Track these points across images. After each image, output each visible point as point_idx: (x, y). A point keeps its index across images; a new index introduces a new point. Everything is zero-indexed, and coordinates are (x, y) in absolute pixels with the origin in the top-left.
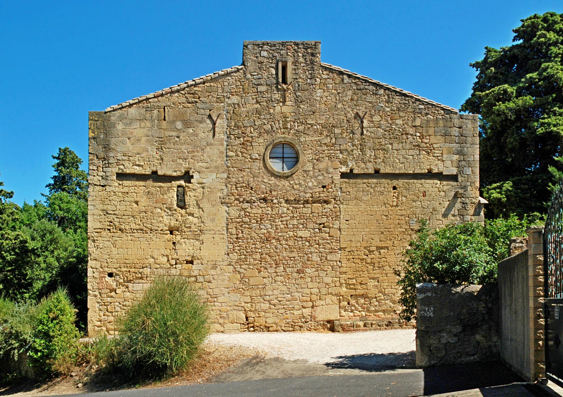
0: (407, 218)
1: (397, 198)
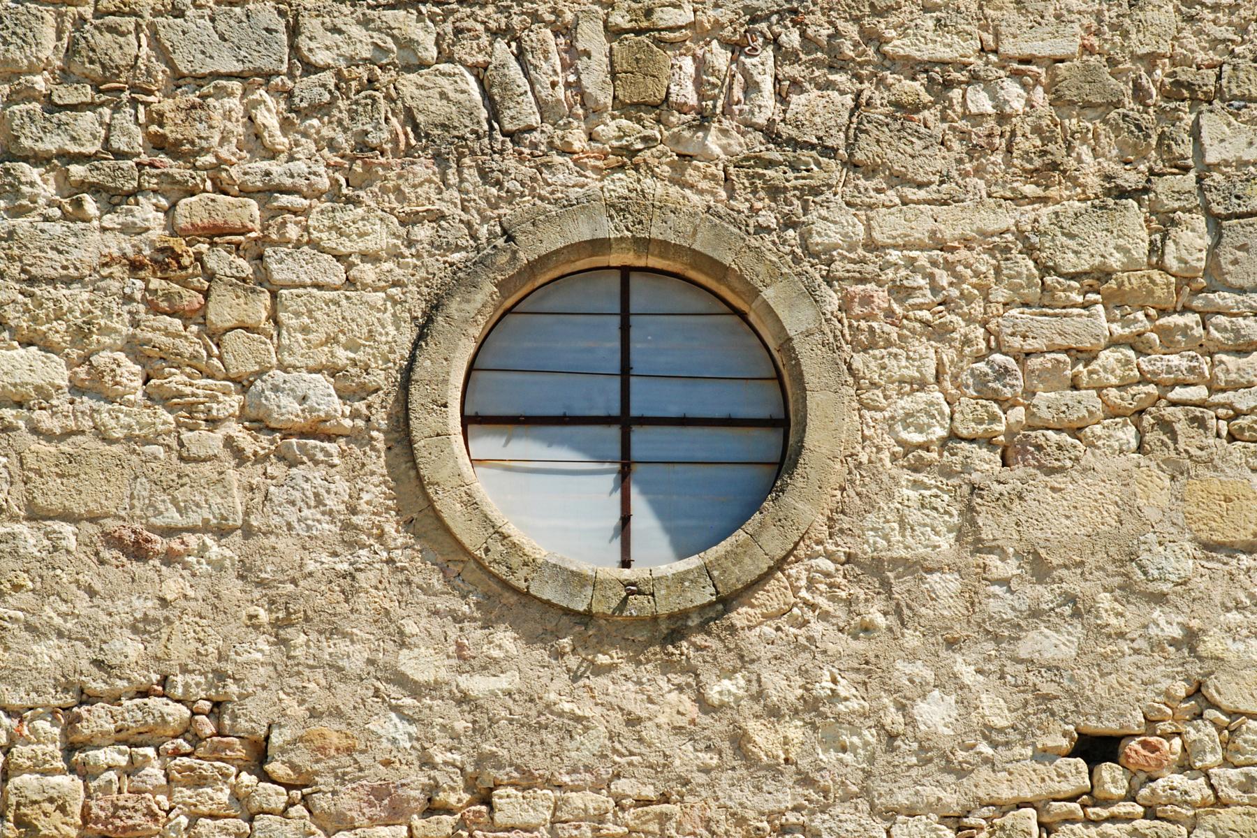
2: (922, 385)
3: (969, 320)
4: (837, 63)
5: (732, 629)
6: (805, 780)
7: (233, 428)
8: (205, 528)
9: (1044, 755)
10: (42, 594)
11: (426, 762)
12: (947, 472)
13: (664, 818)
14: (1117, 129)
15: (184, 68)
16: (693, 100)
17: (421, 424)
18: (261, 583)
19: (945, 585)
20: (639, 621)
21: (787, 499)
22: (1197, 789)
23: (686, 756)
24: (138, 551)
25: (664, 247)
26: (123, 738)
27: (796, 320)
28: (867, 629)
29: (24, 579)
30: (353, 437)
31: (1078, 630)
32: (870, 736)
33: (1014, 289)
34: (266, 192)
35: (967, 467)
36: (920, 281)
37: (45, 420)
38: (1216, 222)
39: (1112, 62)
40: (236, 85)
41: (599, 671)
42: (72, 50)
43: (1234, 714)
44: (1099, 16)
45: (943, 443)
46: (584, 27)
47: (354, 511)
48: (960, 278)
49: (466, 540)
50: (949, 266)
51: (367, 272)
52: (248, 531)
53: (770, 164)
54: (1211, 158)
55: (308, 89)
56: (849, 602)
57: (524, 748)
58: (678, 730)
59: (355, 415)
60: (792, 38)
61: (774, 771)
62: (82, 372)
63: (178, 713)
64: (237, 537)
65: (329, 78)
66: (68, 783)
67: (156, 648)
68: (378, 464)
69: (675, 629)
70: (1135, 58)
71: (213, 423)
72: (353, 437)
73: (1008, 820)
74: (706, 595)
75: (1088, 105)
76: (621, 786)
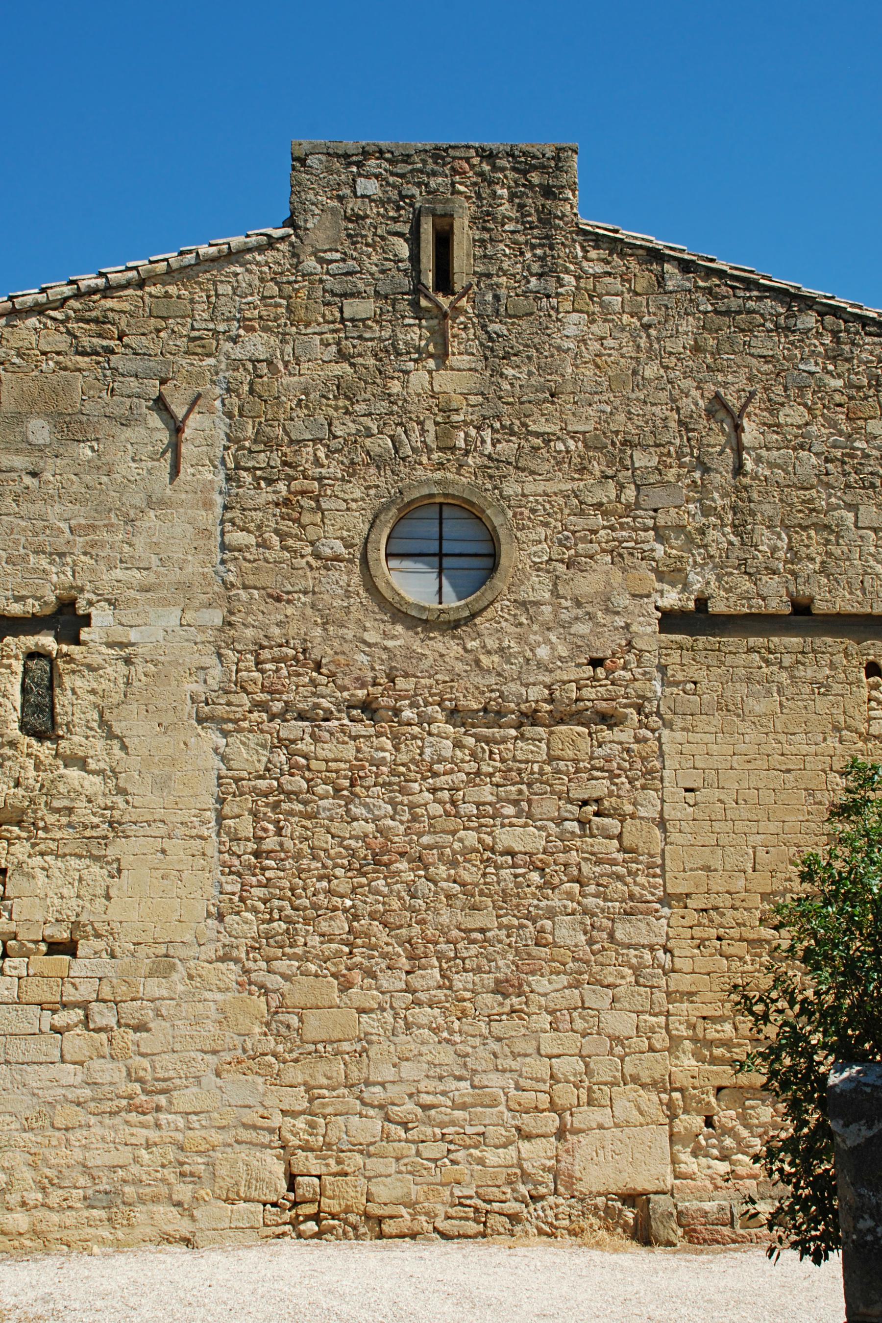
2: (540, 542)
3: (556, 520)
4: (512, 433)
5: (475, 625)
6: (499, 675)
7: (310, 559)
8: (300, 592)
9: (578, 665)
10: (247, 613)
11: (373, 669)
12: (548, 572)
13: (452, 687)
14: (605, 456)
15: (293, 438)
16: (463, 446)
17: (371, 556)
18: (318, 610)
19: (547, 609)
20: (444, 623)
21: (494, 581)
22: (628, 675)
23: (459, 667)
24: (278, 599)
25: (453, 496)
26: (274, 660)
27: (497, 521)
28: (521, 624)
29: (242, 608)
30: (350, 561)
31: (591, 624)
32: (521, 660)
33: (571, 509)
34: (320, 479)
35: (555, 570)
36: (540, 507)
37: (247, 555)
38: (638, 487)
39: (604, 433)
40: (311, 443)
41: (431, 639)
42: (257, 433)
43: (641, 651)
44: (600, 417)
45: (547, 562)
46: (427, 422)
47: (349, 586)
48: (553, 506)
49: (386, 595)
50: (549, 502)
51: (354, 505)
52: (314, 593)
53: (490, 468)
54: (636, 466)
55: (334, 444)
56: (515, 615)
57: (405, 664)
58: (457, 658)
59: (349, 553)
60: (497, 425)
61: (489, 671)
62: (260, 539)
63: (292, 652)
64: (310, 595)
65: (341, 440)
66: (256, 675)
67: (284, 631)
68: (357, 570)
69: (456, 624)
70: (612, 432)
71: (302, 556)
72: (350, 561)
73: (566, 687)
74: (467, 613)
75: (596, 448)
76: (438, 677)
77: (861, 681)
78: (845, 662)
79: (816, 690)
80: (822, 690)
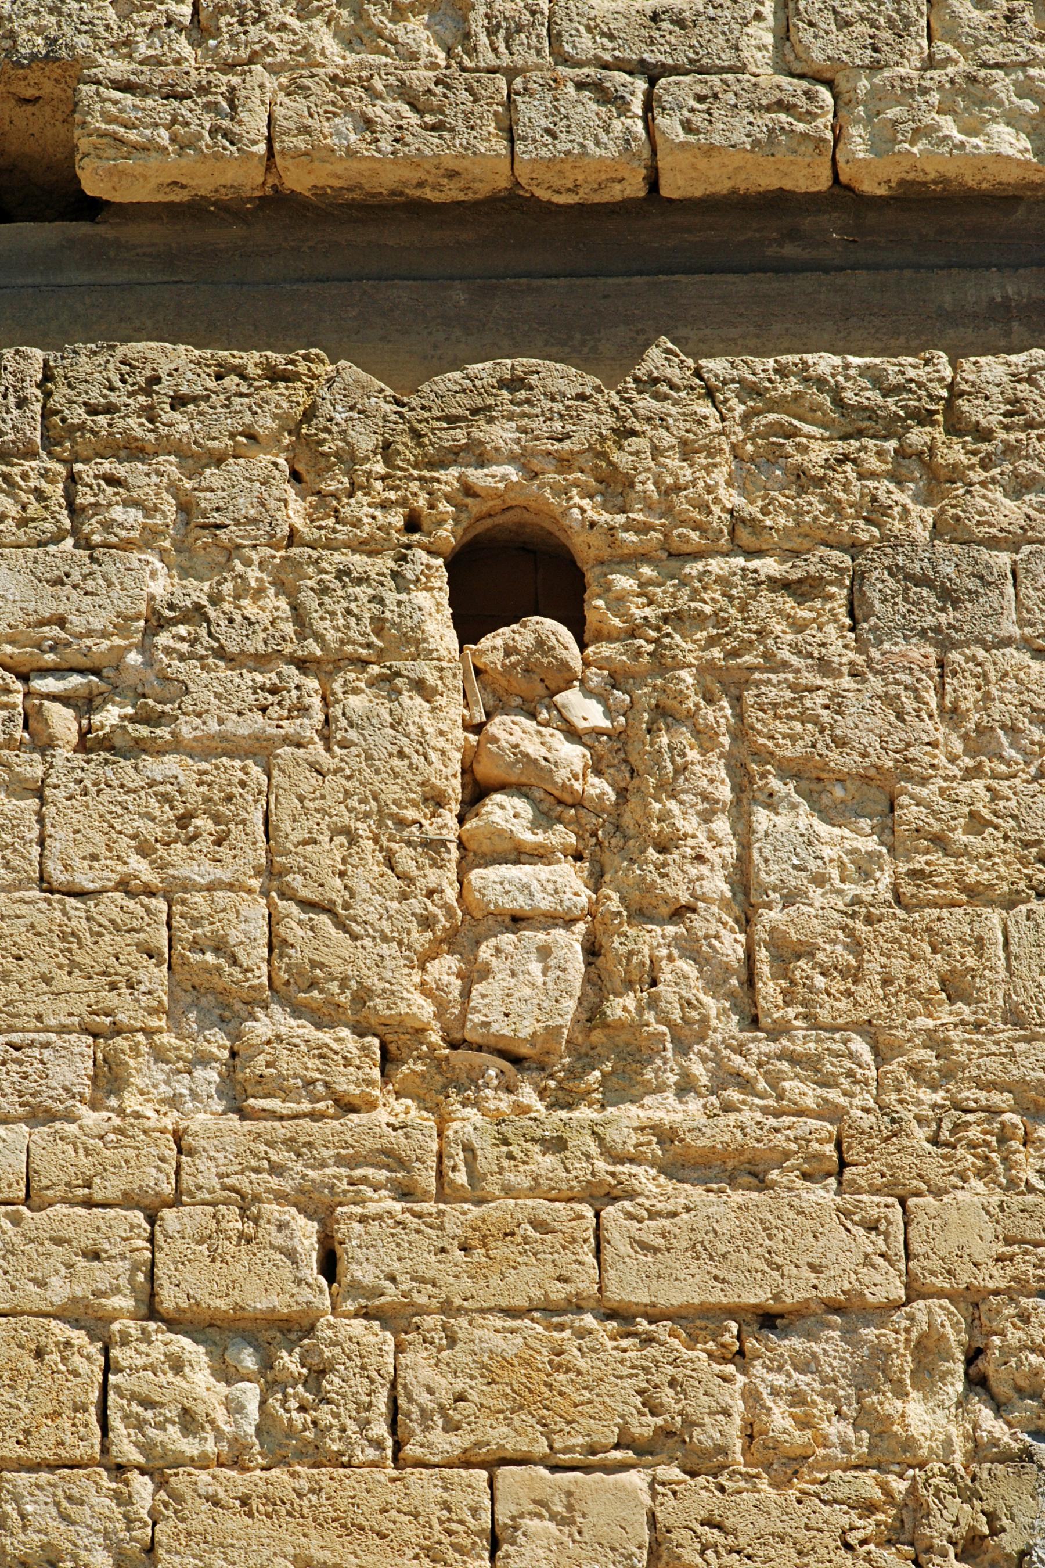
0: (927, 1418)
1: (607, 840)
77: (413, 643)
78: (295, 511)
79: (63, 721)
80: (110, 716)
